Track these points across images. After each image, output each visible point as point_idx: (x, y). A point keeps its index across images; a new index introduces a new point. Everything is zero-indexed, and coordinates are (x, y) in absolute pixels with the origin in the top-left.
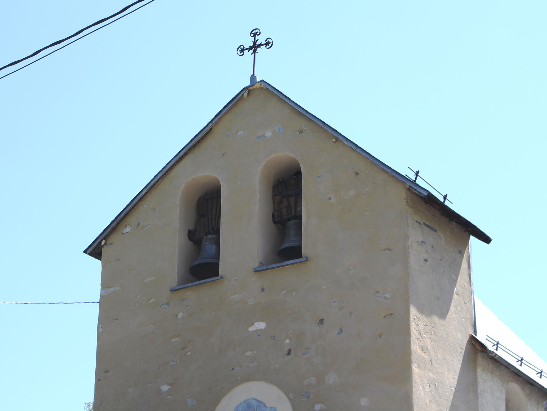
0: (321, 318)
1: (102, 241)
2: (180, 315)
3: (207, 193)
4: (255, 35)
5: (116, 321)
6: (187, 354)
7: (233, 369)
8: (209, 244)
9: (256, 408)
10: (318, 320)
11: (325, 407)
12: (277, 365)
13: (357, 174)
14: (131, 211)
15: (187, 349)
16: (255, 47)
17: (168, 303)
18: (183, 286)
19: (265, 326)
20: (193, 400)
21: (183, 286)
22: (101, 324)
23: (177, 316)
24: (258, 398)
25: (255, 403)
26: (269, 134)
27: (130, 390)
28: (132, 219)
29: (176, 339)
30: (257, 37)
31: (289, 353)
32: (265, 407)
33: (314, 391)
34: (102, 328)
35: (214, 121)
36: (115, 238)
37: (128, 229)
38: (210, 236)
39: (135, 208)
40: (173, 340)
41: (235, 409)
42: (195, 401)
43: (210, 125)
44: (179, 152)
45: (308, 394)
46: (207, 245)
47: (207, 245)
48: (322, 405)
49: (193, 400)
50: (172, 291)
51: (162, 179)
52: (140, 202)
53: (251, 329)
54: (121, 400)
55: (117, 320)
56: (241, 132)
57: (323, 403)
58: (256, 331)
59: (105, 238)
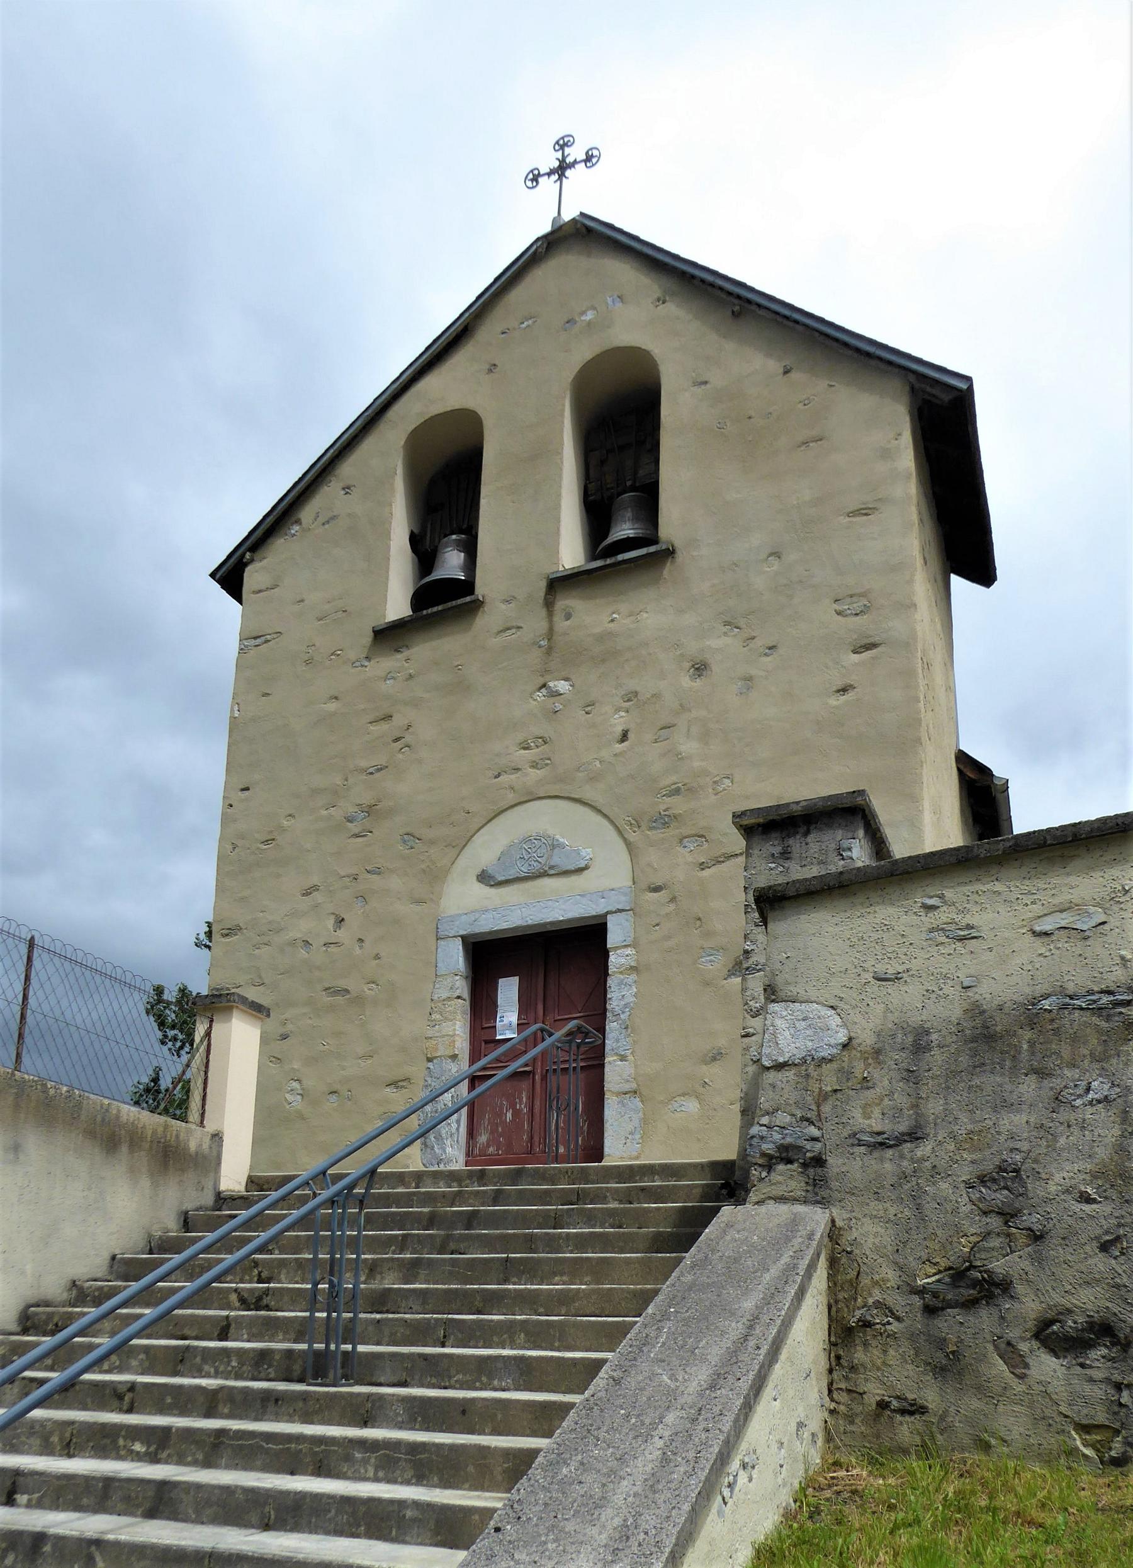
4: (562, 148)
16: (561, 169)
38: (454, 537)
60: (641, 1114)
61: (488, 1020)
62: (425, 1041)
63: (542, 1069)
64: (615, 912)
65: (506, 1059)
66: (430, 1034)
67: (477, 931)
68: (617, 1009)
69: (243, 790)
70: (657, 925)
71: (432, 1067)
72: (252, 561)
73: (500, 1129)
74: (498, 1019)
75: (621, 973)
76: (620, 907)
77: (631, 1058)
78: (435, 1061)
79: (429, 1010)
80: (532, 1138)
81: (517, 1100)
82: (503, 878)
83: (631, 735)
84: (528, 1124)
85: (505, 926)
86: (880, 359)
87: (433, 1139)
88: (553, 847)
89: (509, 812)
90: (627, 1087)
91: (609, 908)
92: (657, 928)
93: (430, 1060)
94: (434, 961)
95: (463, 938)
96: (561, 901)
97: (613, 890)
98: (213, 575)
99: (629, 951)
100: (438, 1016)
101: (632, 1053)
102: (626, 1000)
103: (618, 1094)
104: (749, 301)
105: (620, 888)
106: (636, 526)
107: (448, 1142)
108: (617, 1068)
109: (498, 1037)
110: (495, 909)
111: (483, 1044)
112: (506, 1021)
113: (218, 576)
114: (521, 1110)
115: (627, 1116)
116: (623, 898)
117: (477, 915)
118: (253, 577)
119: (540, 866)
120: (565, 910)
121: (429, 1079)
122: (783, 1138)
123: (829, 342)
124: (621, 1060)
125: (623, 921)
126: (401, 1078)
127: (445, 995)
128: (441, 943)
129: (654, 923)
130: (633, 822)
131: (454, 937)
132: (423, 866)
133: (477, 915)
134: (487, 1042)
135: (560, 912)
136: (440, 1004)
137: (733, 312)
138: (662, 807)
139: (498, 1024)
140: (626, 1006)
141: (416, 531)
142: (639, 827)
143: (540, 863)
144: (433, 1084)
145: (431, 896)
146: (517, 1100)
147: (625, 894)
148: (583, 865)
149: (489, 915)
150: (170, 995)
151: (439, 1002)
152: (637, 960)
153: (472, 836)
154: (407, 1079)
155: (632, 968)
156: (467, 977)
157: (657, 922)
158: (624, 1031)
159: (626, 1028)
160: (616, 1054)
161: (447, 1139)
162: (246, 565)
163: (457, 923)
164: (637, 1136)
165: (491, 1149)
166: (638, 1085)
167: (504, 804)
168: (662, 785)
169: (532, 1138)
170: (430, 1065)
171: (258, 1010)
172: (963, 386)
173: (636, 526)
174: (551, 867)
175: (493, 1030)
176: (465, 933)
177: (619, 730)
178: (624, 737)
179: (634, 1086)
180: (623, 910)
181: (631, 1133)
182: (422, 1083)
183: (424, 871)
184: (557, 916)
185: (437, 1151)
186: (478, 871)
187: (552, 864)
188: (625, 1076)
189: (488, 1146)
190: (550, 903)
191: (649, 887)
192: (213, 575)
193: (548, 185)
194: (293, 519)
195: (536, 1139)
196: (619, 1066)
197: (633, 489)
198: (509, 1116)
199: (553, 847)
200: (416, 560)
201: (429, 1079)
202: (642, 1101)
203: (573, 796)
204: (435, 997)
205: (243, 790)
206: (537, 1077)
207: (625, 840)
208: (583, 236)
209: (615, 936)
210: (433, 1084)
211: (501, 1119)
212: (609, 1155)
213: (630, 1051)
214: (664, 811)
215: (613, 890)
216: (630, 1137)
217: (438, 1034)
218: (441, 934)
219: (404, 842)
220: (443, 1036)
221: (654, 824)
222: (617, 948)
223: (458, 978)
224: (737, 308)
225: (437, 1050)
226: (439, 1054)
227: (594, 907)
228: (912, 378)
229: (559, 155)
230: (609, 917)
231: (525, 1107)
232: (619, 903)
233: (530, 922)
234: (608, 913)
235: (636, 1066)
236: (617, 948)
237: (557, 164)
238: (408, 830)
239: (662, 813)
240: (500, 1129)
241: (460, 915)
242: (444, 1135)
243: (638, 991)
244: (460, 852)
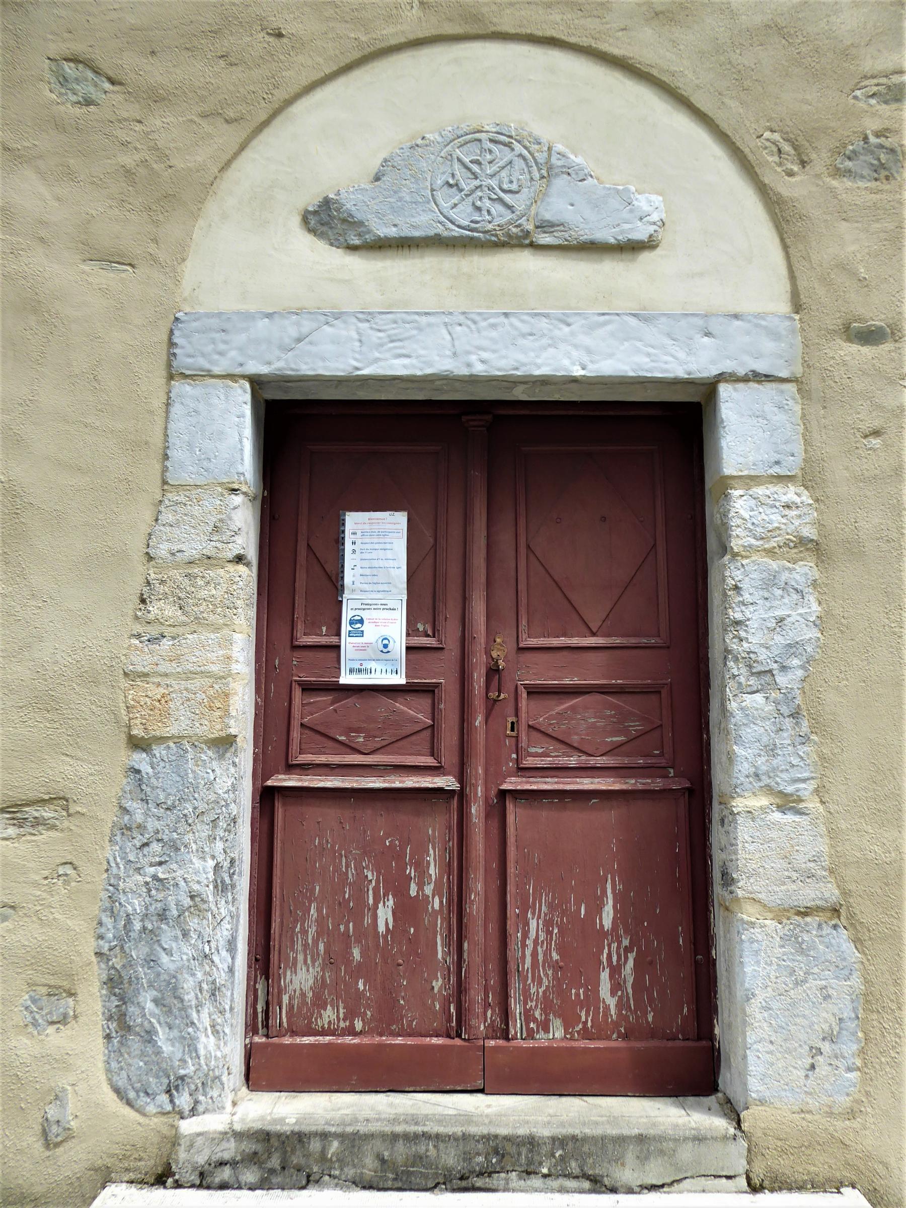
60: (856, 981)
61: (313, 627)
62: (124, 683)
63: (487, 789)
64: (745, 379)
65: (371, 746)
66: (142, 661)
67: (306, 368)
68: (763, 655)
70: (876, 433)
71: (146, 768)
73: (356, 953)
74: (345, 627)
75: (770, 552)
76: (762, 367)
77: (812, 805)
78: (159, 751)
79: (136, 585)
80: (460, 990)
81: (411, 871)
82: (392, 232)
84: (447, 943)
85: (398, 367)
87: (149, 1006)
88: (549, 172)
89: (404, 60)
90: (809, 894)
91: (727, 366)
92: (875, 442)
93: (137, 744)
94: (157, 439)
95: (257, 383)
96: (578, 324)
97: (736, 316)
99: (790, 493)
100: (171, 612)
101: (816, 791)
102: (792, 636)
103: (781, 913)
105: (759, 316)
107: (204, 1019)
108: (774, 834)
109: (346, 679)
110: (367, 316)
111: (297, 693)
112: (371, 633)
114: (422, 902)
115: (813, 983)
116: (768, 345)
117: (307, 325)
119: (509, 216)
120: (589, 351)
121: (134, 806)
124: (782, 809)
125: (769, 408)
126: (32, 795)
127: (194, 547)
128: (180, 387)
129: (865, 427)
130: (787, 147)
131: (232, 377)
132: (128, 160)
133: (307, 325)
134: (308, 688)
135: (575, 354)
136: (176, 574)
138: (871, 125)
139: (348, 643)
142: (803, 163)
143: (509, 207)
144: (152, 824)
145: (152, 248)
146: (411, 871)
147: (775, 336)
148: (641, 233)
149: (347, 331)
150: (902, 574)
151: (177, 566)
152: (819, 524)
153: (289, 102)
154: (61, 800)
155: (802, 542)
156: (255, 498)
157: (877, 424)
158: (788, 723)
159: (795, 715)
160: (769, 790)
161: (199, 1007)
163: (240, 339)
164: (849, 1048)
165: (329, 1015)
166: (845, 893)
167: (391, 33)
168: (868, 65)
169: (460, 990)
170: (140, 760)
174: (544, 226)
175: (332, 655)
176: (264, 370)
179: (830, 892)
180: (768, 378)
181: (830, 1038)
182: (109, 817)
183: (128, 173)
184: (566, 362)
185: (166, 1048)
186: (310, 199)
187: (548, 216)
188: (801, 861)
189: (320, 1003)
190: (543, 323)
191: (847, 328)
195: (476, 995)
196: (780, 827)
198: (385, 915)
199: (549, 172)
201: (134, 806)
202: (857, 941)
203: (604, 47)
204: (162, 550)
206: (476, 810)
207: (763, 190)
210: (152, 824)
211: (358, 924)
212: (762, 1102)
213: (811, 786)
214: (877, 135)
215: (736, 316)
216: (826, 1047)
217: (164, 667)
218: (183, 361)
219: (64, 81)
220: (189, 675)
221: (849, 164)
222: (752, 480)
223: (238, 500)
225: (166, 714)
226: (172, 730)
227: (682, 355)
230: (725, 391)
231: (437, 891)
232: (758, 356)
233: (479, 369)
234: (721, 377)
235: (833, 834)
236: (752, 480)
238: (78, 47)
239: (873, 140)
240: (356, 953)
241: (248, 317)
242: (190, 998)
243: (828, 612)
244: (243, 147)
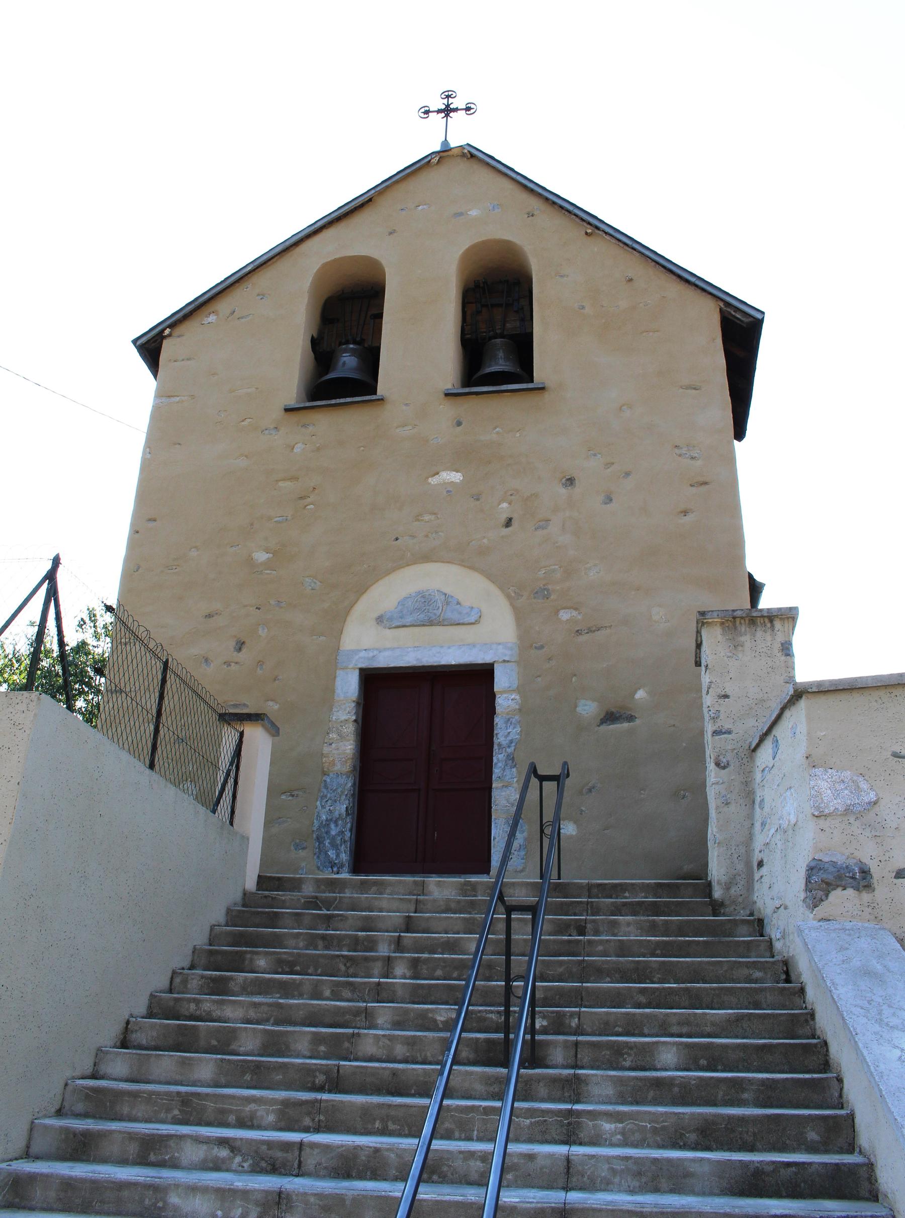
0: (569, 477)
1: (165, 329)
2: (298, 449)
3: (343, 291)
4: (448, 97)
5: (177, 446)
6: (308, 507)
7: (397, 539)
8: (350, 356)
9: (440, 605)
10: (564, 479)
11: (579, 617)
12: (485, 541)
13: (631, 280)
14: (220, 295)
15: (309, 500)
16: (447, 111)
17: (276, 428)
18: (308, 404)
19: (461, 478)
20: (315, 580)
21: (467, 390)
22: (149, 447)
23: (293, 449)
24: (445, 591)
25: (440, 598)
26: (474, 213)
27: (194, 553)
28: (224, 306)
29: (288, 484)
30: (451, 100)
31: (507, 523)
32: (459, 606)
33: (558, 588)
34: (150, 453)
35: (378, 189)
36: (190, 329)
37: (212, 318)
38: (351, 346)
39: (228, 290)
40: (281, 484)
41: (808, 881)
42: (319, 583)
43: (373, 192)
44: (316, 222)
45: (546, 593)
46: (344, 356)
47: (344, 356)
48: (574, 613)
49: (315, 580)
50: (288, 410)
51: (278, 257)
52: (237, 285)
53: (433, 481)
54: (174, 567)
55: (179, 444)
56: (425, 207)
57: (576, 609)
58: (445, 484)
59: (170, 326)
69: (150, 520)
72: (170, 335)
83: (515, 523)
86: (696, 286)
98: (134, 342)
104: (597, 228)
106: (508, 363)
113: (139, 343)
116: (508, 652)
117: (375, 652)
118: (168, 349)
122: (838, 871)
123: (607, 237)
137: (586, 233)
140: (511, 742)
141: (315, 336)
149: (387, 653)
162: (165, 337)
171: (274, 730)
172: (759, 316)
173: (508, 363)
177: (503, 517)
178: (509, 523)
192: (134, 342)
193: (437, 119)
194: (211, 310)
197: (502, 336)
200: (314, 356)
205: (150, 520)
208: (468, 159)
209: (502, 680)
222: (504, 692)
224: (589, 231)
228: (722, 305)
229: (445, 101)
236: (504, 692)
237: (444, 107)
241: (360, 651)
